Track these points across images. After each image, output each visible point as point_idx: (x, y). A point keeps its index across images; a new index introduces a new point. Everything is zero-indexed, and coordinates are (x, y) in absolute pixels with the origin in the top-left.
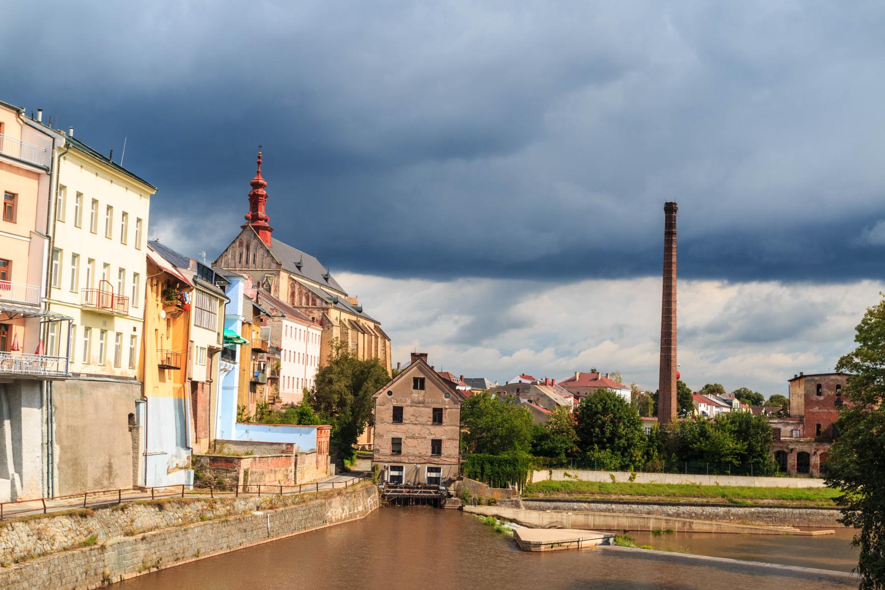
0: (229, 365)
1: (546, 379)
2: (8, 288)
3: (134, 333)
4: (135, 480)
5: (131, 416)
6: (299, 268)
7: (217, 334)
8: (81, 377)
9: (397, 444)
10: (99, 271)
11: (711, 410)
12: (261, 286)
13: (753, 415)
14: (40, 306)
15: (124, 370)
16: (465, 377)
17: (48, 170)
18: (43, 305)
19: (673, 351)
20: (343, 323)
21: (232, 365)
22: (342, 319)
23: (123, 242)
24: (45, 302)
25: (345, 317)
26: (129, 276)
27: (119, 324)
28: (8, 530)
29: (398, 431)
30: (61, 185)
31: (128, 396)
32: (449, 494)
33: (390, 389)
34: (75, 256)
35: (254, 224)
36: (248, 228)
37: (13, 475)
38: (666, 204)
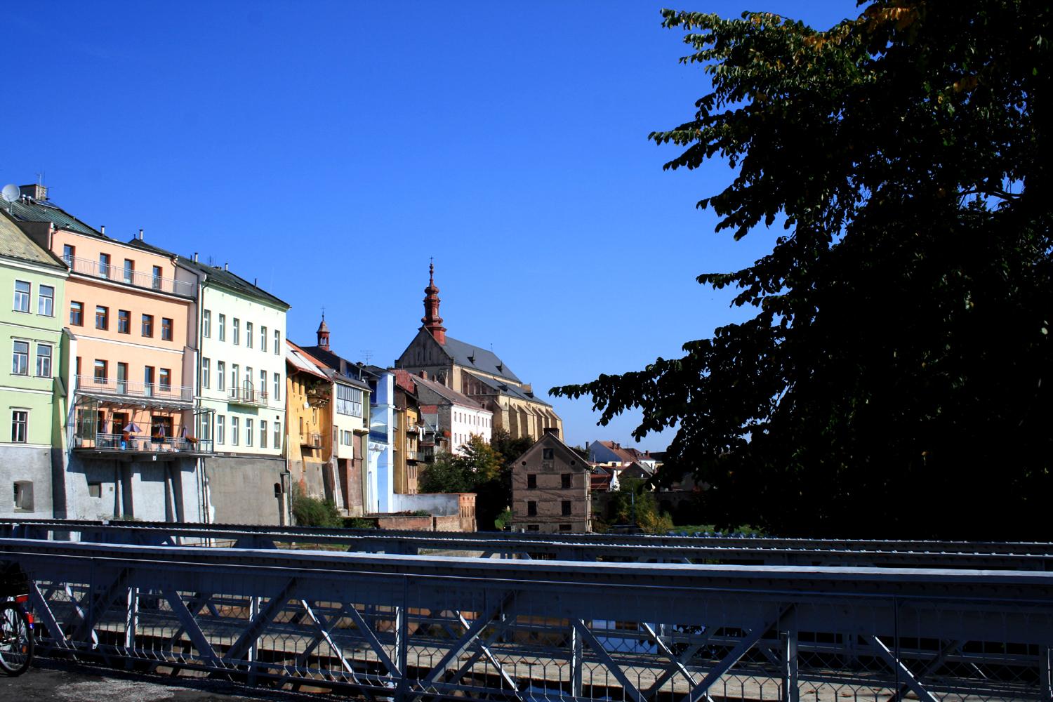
0: (381, 446)
2: (105, 383)
3: (277, 421)
5: (277, 486)
6: (471, 359)
7: (362, 420)
8: (232, 455)
9: (532, 507)
10: (243, 374)
13: (796, 452)
14: (192, 402)
15: (271, 450)
16: (650, 452)
17: (195, 300)
18: (195, 401)
21: (384, 446)
22: (512, 404)
23: (264, 348)
25: (515, 402)
26: (270, 377)
27: (263, 414)
29: (533, 495)
31: (274, 469)
33: (524, 460)
34: (221, 363)
35: (429, 326)
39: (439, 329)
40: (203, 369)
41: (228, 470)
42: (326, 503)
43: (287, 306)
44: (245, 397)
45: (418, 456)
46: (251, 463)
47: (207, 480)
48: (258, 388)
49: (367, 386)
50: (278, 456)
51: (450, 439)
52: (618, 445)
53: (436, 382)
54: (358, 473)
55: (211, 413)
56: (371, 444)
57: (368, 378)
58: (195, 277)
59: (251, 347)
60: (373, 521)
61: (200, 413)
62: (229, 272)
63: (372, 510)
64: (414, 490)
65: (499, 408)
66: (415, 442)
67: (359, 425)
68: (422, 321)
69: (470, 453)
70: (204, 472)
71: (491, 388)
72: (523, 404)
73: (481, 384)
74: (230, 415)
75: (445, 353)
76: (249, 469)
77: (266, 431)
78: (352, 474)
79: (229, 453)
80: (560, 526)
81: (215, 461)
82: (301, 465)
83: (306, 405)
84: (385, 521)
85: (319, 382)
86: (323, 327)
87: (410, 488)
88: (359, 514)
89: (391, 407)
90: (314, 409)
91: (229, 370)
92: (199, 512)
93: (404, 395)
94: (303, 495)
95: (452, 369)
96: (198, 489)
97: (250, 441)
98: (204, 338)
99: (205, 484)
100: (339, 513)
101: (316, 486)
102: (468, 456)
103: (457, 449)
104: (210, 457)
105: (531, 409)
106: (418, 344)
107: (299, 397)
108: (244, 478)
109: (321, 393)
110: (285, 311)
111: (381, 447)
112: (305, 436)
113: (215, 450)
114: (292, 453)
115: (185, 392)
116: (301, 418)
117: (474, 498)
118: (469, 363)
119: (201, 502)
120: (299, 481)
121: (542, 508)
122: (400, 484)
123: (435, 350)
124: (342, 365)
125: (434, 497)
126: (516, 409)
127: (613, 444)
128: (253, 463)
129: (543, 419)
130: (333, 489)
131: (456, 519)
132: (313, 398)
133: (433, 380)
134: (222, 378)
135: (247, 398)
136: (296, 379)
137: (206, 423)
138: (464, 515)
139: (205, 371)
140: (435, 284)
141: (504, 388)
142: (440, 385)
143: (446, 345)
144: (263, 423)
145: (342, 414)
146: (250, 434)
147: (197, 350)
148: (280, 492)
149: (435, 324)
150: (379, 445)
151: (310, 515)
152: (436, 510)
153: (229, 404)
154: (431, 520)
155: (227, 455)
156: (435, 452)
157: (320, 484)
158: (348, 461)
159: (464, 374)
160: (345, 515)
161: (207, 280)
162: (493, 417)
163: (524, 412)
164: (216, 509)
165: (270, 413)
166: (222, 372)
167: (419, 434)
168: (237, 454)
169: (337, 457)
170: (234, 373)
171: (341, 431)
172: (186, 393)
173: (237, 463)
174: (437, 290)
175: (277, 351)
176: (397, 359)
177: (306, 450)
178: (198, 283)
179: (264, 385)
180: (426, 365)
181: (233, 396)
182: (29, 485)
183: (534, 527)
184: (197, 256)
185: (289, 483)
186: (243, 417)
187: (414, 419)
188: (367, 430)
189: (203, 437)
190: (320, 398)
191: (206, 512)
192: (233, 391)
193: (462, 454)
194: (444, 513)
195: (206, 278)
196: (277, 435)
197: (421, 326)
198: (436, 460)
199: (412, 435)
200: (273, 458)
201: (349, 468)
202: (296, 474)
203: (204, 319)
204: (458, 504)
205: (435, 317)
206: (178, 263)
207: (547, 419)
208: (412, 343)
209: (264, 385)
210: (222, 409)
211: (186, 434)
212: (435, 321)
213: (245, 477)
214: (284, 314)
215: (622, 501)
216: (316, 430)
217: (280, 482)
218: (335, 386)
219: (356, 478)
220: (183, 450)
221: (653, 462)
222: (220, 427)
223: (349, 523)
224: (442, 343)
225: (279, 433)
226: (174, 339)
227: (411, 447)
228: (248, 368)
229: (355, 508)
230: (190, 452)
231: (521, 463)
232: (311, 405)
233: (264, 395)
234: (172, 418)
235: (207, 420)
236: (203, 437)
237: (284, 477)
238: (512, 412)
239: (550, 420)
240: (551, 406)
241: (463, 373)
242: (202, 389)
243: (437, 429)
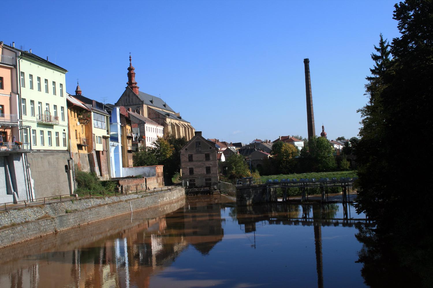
0: (115, 144)
1: (267, 140)
3: (64, 132)
4: (71, 192)
5: (66, 166)
6: (151, 102)
8: (41, 151)
9: (191, 171)
10: (44, 108)
11: (339, 147)
12: (135, 112)
14: (17, 123)
15: (62, 147)
17: (15, 66)
18: (19, 122)
19: (312, 122)
20: (173, 124)
21: (117, 144)
23: (55, 93)
24: (20, 121)
25: (174, 121)
27: (56, 129)
28: (9, 214)
30: (21, 72)
31: (64, 158)
32: (214, 189)
33: (186, 148)
36: (128, 88)
37: (14, 193)
38: (304, 59)
39: (136, 87)
40: (22, 104)
41: (40, 159)
42: (91, 174)
43: (66, 71)
44: (46, 119)
45: (132, 148)
46: (51, 155)
47: (29, 165)
48: (53, 114)
49: (107, 113)
50: (65, 151)
51: (145, 140)
52: (218, 140)
53: (136, 113)
54: (105, 158)
55: (28, 129)
56: (111, 143)
57: (109, 110)
58: (14, 53)
59: (26, 115)
60: (116, 182)
61: (22, 129)
62: (32, 54)
63: (113, 177)
64: (131, 165)
65: (167, 124)
66: (130, 141)
67: (105, 133)
68: (127, 84)
69: (157, 146)
70: (27, 161)
71: (162, 115)
72: (177, 122)
73: (157, 113)
74: (38, 129)
75: (139, 99)
76: (50, 158)
77: (58, 138)
78: (103, 158)
79: (40, 150)
80: (205, 179)
81: (33, 154)
82: (78, 155)
83: (78, 123)
84: (122, 181)
85: (84, 111)
86: (78, 88)
87: (130, 164)
88: (107, 178)
89: (119, 124)
90: (82, 126)
91: (37, 105)
92: (25, 183)
93: (125, 119)
94: (80, 170)
95: (143, 106)
96: (24, 170)
97: (50, 143)
98: (21, 88)
99: (27, 167)
100: (99, 179)
101: (85, 165)
102: (157, 147)
103: (149, 144)
104: (30, 152)
105: (181, 124)
106: (126, 95)
107: (75, 121)
108: (48, 163)
109: (86, 117)
110: (64, 73)
111: (116, 144)
112: (79, 139)
113: (32, 149)
114: (73, 149)
115: (13, 118)
116: (76, 130)
117: (162, 167)
118: (164, 107)
119: (26, 177)
120: (77, 163)
121: (196, 171)
122: (125, 162)
123: (134, 97)
124: (94, 103)
125: (143, 168)
126: (174, 124)
127: (216, 140)
128: (53, 155)
129: (187, 129)
130: (94, 166)
131: (155, 178)
132: (81, 120)
133: (134, 112)
134: (33, 109)
135: (47, 120)
136: (72, 110)
137: (26, 134)
138: (158, 176)
139: (23, 106)
140: (133, 65)
141: (168, 115)
142: (138, 114)
143: (139, 95)
144: (57, 133)
145: (100, 128)
146: (50, 139)
147: (18, 94)
148: (68, 170)
149: (134, 85)
150: (115, 143)
151: (85, 181)
152: (145, 174)
153: (37, 123)
154: (144, 180)
155: (39, 151)
156: (139, 146)
157: (87, 164)
158: (100, 152)
159: (149, 109)
160: (102, 179)
161: (21, 55)
162: (164, 128)
163: (178, 126)
164: (35, 181)
165: (60, 128)
166: (32, 106)
167: (132, 138)
168: (44, 150)
169: (95, 150)
170: (39, 107)
171: (97, 136)
172: (13, 119)
173: (44, 155)
174: (133, 68)
175: (62, 95)
176: (116, 103)
177: (80, 147)
178: (16, 57)
179: (56, 113)
180: (130, 105)
181: (40, 119)
182: (211, 180)
183: (192, 180)
184: (14, 44)
185: (72, 164)
186: (46, 130)
187: (129, 130)
188: (109, 136)
189: (24, 142)
190: (85, 120)
191: (29, 183)
192: (40, 116)
193: (154, 146)
194: (149, 176)
195: (20, 54)
196: (64, 140)
197: (126, 86)
198: (139, 150)
199: (130, 138)
200: (63, 151)
201: (101, 155)
202: (76, 160)
203: (21, 77)
204: (155, 171)
205: (133, 82)
206: (4, 46)
207: (188, 129)
208: (123, 94)
209: (56, 113)
210: (34, 126)
211: (15, 140)
212: (133, 84)
213: (49, 163)
214: (64, 75)
215: (232, 166)
216: (83, 136)
217: (67, 164)
218: (92, 113)
219: (104, 161)
220: (14, 149)
221: (234, 148)
222: (34, 136)
223: (104, 183)
224: (137, 94)
225: (65, 138)
226: (4, 88)
227: (129, 143)
228: (47, 104)
229: (105, 175)
230: (18, 150)
231: (185, 149)
232: (81, 123)
233: (56, 118)
234: (6, 132)
235: (26, 133)
236: (24, 142)
237: (70, 161)
238: (172, 125)
239: (190, 129)
240: (189, 123)
241: (148, 108)
242: (22, 115)
243: (139, 135)
